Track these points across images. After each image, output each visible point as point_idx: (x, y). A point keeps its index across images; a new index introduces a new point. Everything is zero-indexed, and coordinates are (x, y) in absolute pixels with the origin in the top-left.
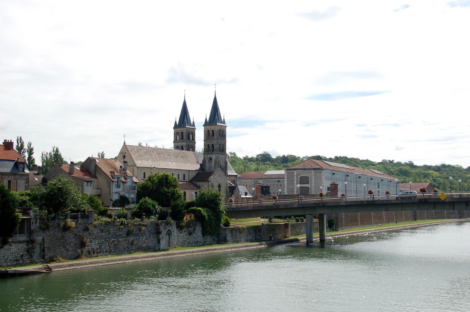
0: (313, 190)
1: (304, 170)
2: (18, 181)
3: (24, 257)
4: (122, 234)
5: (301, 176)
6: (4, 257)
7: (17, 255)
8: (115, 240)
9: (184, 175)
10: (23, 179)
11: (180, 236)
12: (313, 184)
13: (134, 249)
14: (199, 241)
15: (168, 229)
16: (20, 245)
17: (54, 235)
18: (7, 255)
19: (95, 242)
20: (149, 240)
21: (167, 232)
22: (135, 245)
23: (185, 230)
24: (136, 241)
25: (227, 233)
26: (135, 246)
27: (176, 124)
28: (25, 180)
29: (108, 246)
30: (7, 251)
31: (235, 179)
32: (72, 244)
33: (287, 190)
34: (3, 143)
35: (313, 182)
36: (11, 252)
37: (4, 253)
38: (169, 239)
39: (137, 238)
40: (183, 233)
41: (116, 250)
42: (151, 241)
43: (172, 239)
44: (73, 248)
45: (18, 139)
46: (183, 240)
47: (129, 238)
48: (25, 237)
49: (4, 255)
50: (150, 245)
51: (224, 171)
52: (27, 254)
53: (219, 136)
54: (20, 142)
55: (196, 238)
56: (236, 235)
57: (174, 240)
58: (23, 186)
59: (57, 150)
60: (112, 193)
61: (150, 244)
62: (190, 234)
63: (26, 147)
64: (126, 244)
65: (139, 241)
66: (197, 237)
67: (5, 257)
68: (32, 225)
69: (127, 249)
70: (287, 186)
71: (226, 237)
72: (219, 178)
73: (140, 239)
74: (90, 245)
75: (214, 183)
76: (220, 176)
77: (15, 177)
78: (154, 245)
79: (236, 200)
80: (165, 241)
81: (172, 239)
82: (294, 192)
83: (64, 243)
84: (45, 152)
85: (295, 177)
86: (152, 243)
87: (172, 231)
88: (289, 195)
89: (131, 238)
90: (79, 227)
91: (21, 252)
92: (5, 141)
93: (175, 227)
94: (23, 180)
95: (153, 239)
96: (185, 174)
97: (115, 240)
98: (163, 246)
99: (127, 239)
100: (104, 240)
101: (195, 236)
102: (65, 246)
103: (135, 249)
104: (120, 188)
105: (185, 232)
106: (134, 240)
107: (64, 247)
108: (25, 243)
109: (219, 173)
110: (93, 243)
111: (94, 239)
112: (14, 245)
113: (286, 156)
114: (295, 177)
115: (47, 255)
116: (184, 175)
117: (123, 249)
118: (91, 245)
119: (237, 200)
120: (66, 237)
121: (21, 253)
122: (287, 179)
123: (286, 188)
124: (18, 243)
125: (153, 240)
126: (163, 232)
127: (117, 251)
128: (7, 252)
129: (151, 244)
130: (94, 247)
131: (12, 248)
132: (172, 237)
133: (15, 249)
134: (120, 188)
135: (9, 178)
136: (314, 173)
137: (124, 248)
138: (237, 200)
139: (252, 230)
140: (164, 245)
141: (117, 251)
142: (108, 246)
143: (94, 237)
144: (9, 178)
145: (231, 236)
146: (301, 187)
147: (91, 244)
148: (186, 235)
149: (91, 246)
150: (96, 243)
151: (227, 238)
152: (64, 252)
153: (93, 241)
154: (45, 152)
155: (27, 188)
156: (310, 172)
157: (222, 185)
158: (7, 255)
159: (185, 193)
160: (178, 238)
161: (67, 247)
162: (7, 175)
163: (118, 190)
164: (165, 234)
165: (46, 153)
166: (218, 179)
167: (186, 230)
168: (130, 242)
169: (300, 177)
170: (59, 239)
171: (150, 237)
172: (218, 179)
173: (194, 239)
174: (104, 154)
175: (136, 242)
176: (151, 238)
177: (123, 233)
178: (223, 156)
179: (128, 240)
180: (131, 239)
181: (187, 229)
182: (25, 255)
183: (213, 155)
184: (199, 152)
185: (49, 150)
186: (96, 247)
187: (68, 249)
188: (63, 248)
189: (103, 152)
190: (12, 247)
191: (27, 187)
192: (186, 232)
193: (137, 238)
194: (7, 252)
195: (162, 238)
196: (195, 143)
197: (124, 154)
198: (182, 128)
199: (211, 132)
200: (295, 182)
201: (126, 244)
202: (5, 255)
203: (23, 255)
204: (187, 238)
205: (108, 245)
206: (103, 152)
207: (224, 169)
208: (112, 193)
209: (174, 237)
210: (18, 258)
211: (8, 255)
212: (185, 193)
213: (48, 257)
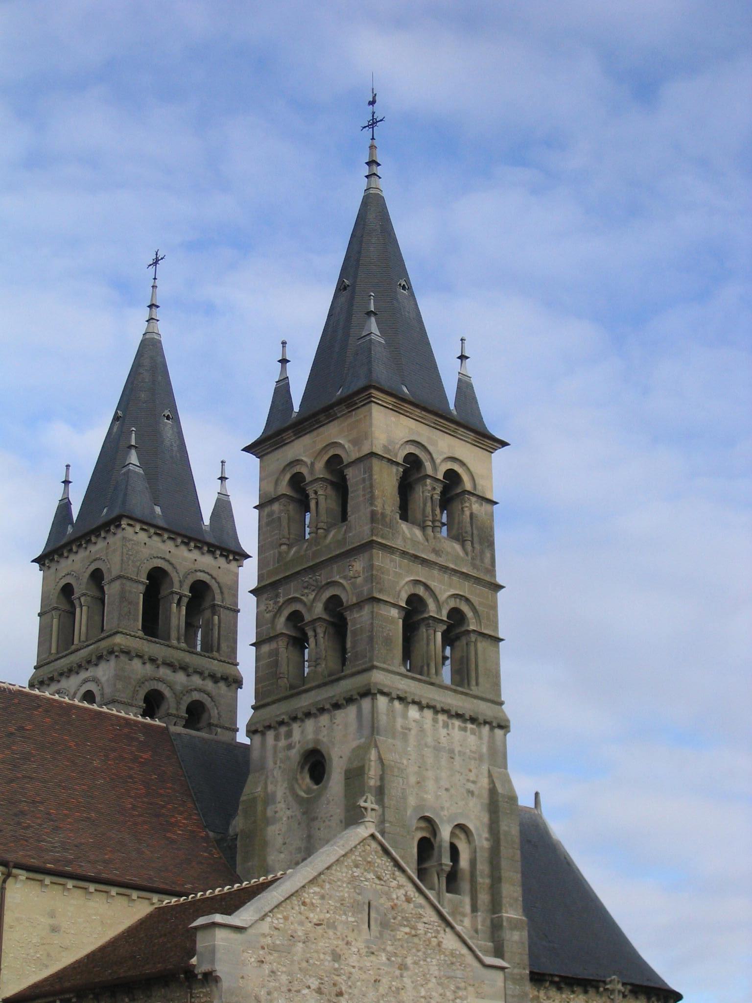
51: (484, 898)
72: (359, 945)
166: (336, 957)
172: (336, 957)
178: (457, 734)
183: (340, 714)
207: (483, 881)
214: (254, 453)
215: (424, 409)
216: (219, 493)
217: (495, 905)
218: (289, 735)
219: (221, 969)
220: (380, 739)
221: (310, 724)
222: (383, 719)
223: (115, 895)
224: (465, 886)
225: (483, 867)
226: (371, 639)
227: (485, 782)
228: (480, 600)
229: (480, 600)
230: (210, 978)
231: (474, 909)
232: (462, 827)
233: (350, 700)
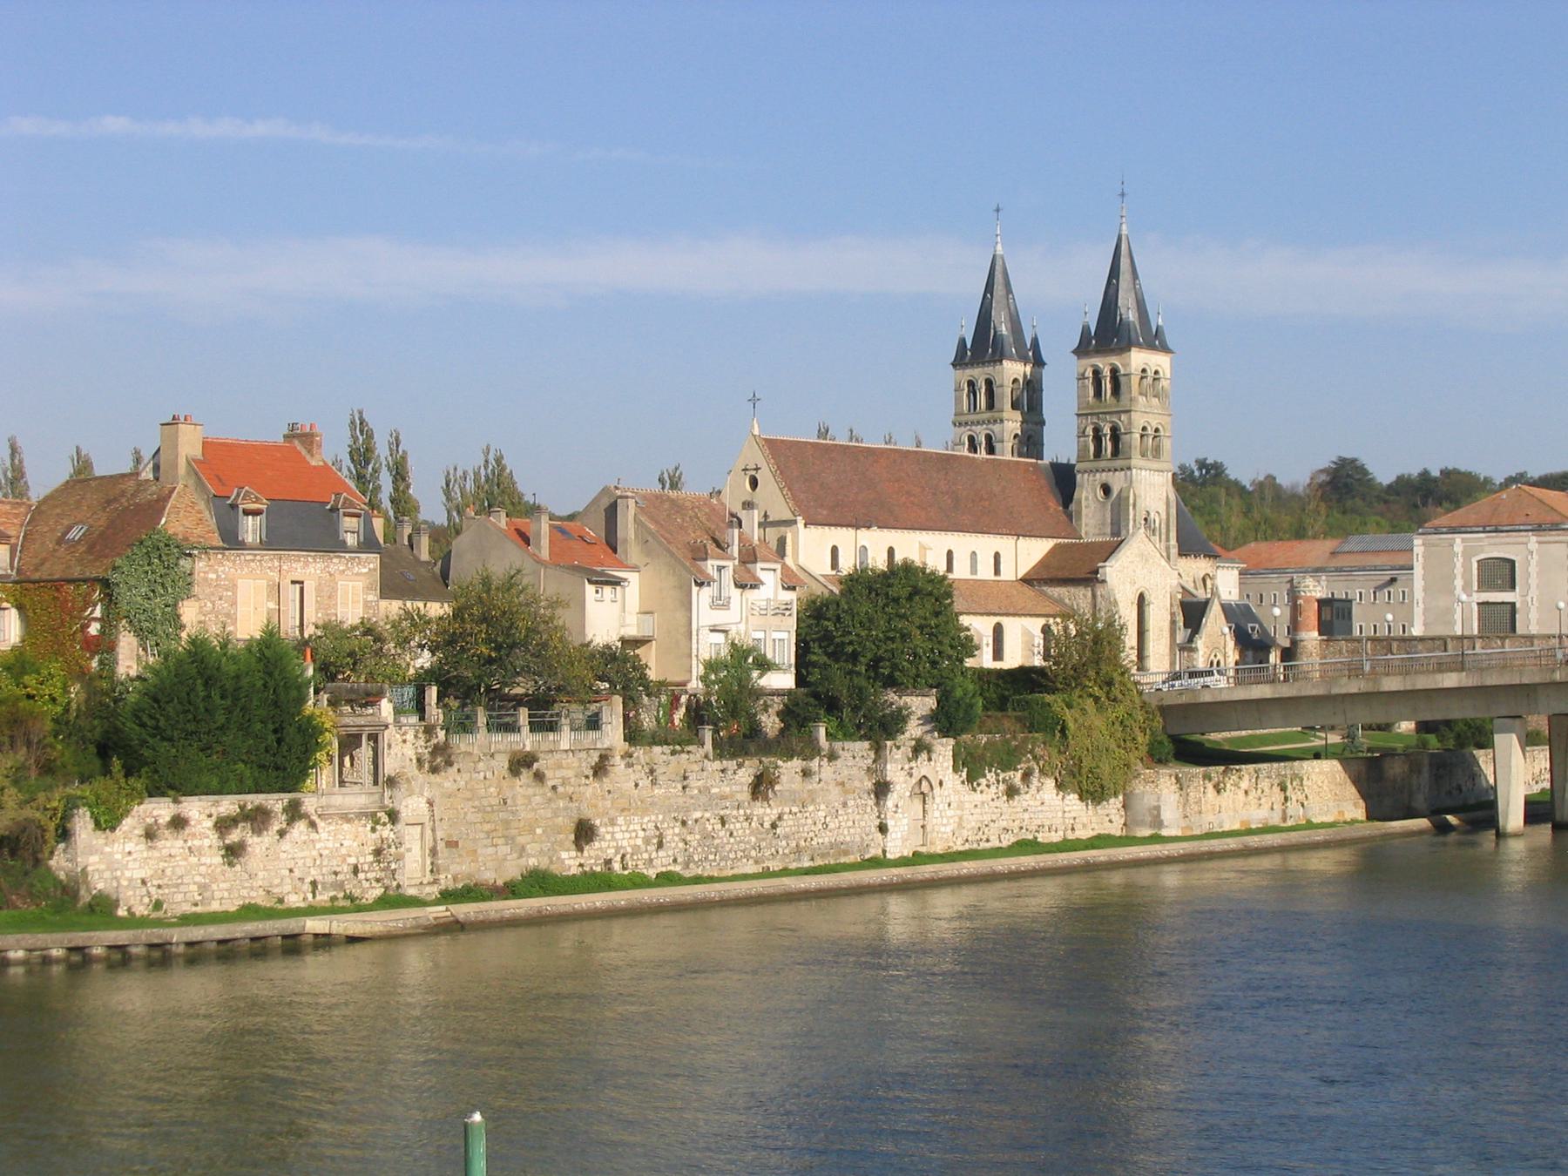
0: (1534, 615)
1: (1494, 534)
2: (340, 583)
3: (361, 876)
4: (732, 795)
5: (1482, 556)
6: (291, 871)
7: (338, 866)
8: (707, 815)
9: (997, 556)
10: (357, 574)
11: (967, 805)
12: (1534, 592)
13: (781, 852)
14: (1047, 823)
15: (917, 775)
16: (346, 826)
17: (468, 794)
18: (300, 863)
19: (629, 823)
20: (841, 818)
21: (913, 788)
22: (787, 837)
23: (988, 780)
24: (791, 823)
25: (1165, 791)
26: (784, 843)
27: (966, 346)
28: (363, 578)
29: (676, 839)
30: (303, 850)
31: (1209, 571)
32: (539, 831)
33: (1423, 618)
34: (285, 436)
35: (1533, 581)
36: (315, 853)
37: (290, 856)
38: (924, 817)
39: (795, 809)
40: (982, 792)
41: (711, 857)
42: (850, 823)
43: (937, 814)
44: (543, 845)
45: (353, 423)
46: (982, 822)
47: (761, 811)
48: (363, 796)
49: (291, 864)
50: (848, 839)
51: (1163, 537)
52: (372, 863)
53: (1141, 394)
54: (362, 432)
55: (1034, 813)
56: (1199, 802)
57: (945, 821)
58: (359, 602)
59: (499, 460)
60: (698, 631)
61: (846, 832)
62: (1012, 792)
63: (382, 450)
64: (750, 835)
65: (803, 821)
66: (1040, 808)
67: (297, 873)
68: (389, 754)
69: (753, 853)
70: (1424, 599)
71: (1158, 808)
72: (1140, 567)
73: (808, 814)
74: (608, 833)
75: (1121, 587)
76: (1144, 558)
77: (328, 566)
78: (862, 837)
79: (1212, 657)
80: (905, 821)
81: (937, 814)
82: (1453, 623)
83: (507, 823)
84: (455, 469)
85: (1459, 562)
86: (852, 831)
87: (935, 784)
88: (1433, 639)
89: (768, 811)
90: (564, 766)
91: (350, 856)
92: (294, 434)
93: (948, 768)
94: (359, 578)
95: (858, 813)
96: (1001, 553)
97: (707, 815)
98: (899, 843)
99: (751, 814)
100: (661, 817)
101: (1031, 803)
102: (513, 839)
103: (784, 854)
104: (729, 609)
105: (988, 786)
106: (780, 818)
107: (510, 840)
108: (363, 822)
109: (1139, 547)
110: (617, 829)
111: (623, 810)
112: (324, 829)
113: (1435, 473)
114: (1459, 562)
115: (447, 870)
116: (997, 556)
117: (740, 854)
118: (613, 833)
119: (1215, 656)
120: (514, 801)
121: (352, 860)
122: (1424, 568)
123: (1418, 611)
124: (340, 822)
125: (858, 817)
126: (898, 787)
127: (715, 860)
128: (306, 853)
129: (849, 834)
130: (625, 843)
131: (320, 840)
132: (935, 806)
133: (330, 845)
134: (729, 609)
135: (308, 571)
136: (1537, 545)
137: (743, 851)
138: (1215, 656)
139: (1267, 780)
140: (904, 840)
141: (715, 860)
142: (676, 839)
143: (623, 803)
144: (308, 571)
145: (1181, 807)
146: (1483, 603)
147: (610, 829)
148: (993, 800)
149: (613, 839)
150: (631, 827)
151: (1162, 813)
152: (509, 857)
153: (620, 820)
154: (455, 469)
155: (371, 611)
156: (1520, 540)
157: (1153, 596)
158: (300, 863)
159: (998, 631)
160: (959, 812)
161: (521, 840)
162: (299, 561)
163: (720, 618)
164: (908, 794)
165: (460, 473)
166: (1134, 571)
167: (993, 780)
168: (767, 825)
169: (1478, 562)
170: (489, 809)
171: (845, 805)
173: (1026, 816)
174: (681, 474)
175: (791, 826)
176: (850, 811)
177: (738, 788)
178: (1156, 477)
179: (755, 819)
180: (768, 815)
181: (997, 775)
182: (366, 867)
183: (1117, 473)
184: (62, 472)
185: (471, 462)
186: (632, 842)
187: (523, 849)
188: (507, 844)
189: (677, 469)
190: (318, 837)
191: (370, 608)
192: (993, 788)
193: (795, 809)
194: (306, 853)
195: (896, 812)
196: (1043, 423)
197: (753, 473)
198: (989, 362)
199: (1150, 374)
200: (1459, 583)
201: (750, 835)
202: (293, 862)
203: (360, 866)
204: (996, 810)
205: (677, 835)
206: (677, 469)
207: (1164, 531)
208: (698, 631)
209: (941, 806)
210: (340, 877)
211: (304, 864)
212: (998, 631)
213: (449, 876)
214: (225, 791)
215: (422, 833)
216: (1078, 415)
217: (1168, 539)
218: (1094, 476)
219: (1108, 579)
220: (1134, 485)
221: (1104, 474)
222: (1134, 478)
223: (1048, 456)
224: (1157, 533)
225: (1163, 526)
226: (1130, 447)
227: (1165, 494)
228: (304, 452)
229: (304, 452)
230: (1104, 581)
231: (1160, 541)
232: (1158, 512)
233: (1122, 470)
